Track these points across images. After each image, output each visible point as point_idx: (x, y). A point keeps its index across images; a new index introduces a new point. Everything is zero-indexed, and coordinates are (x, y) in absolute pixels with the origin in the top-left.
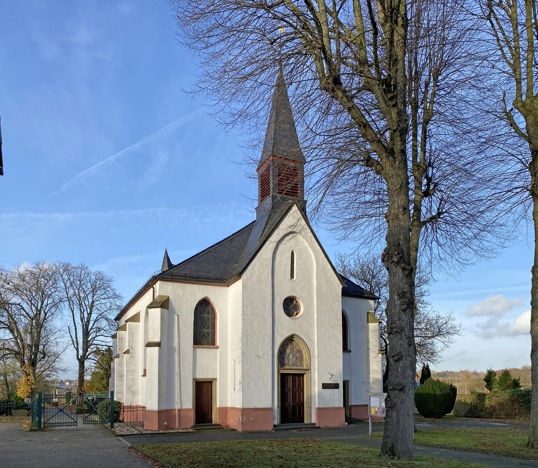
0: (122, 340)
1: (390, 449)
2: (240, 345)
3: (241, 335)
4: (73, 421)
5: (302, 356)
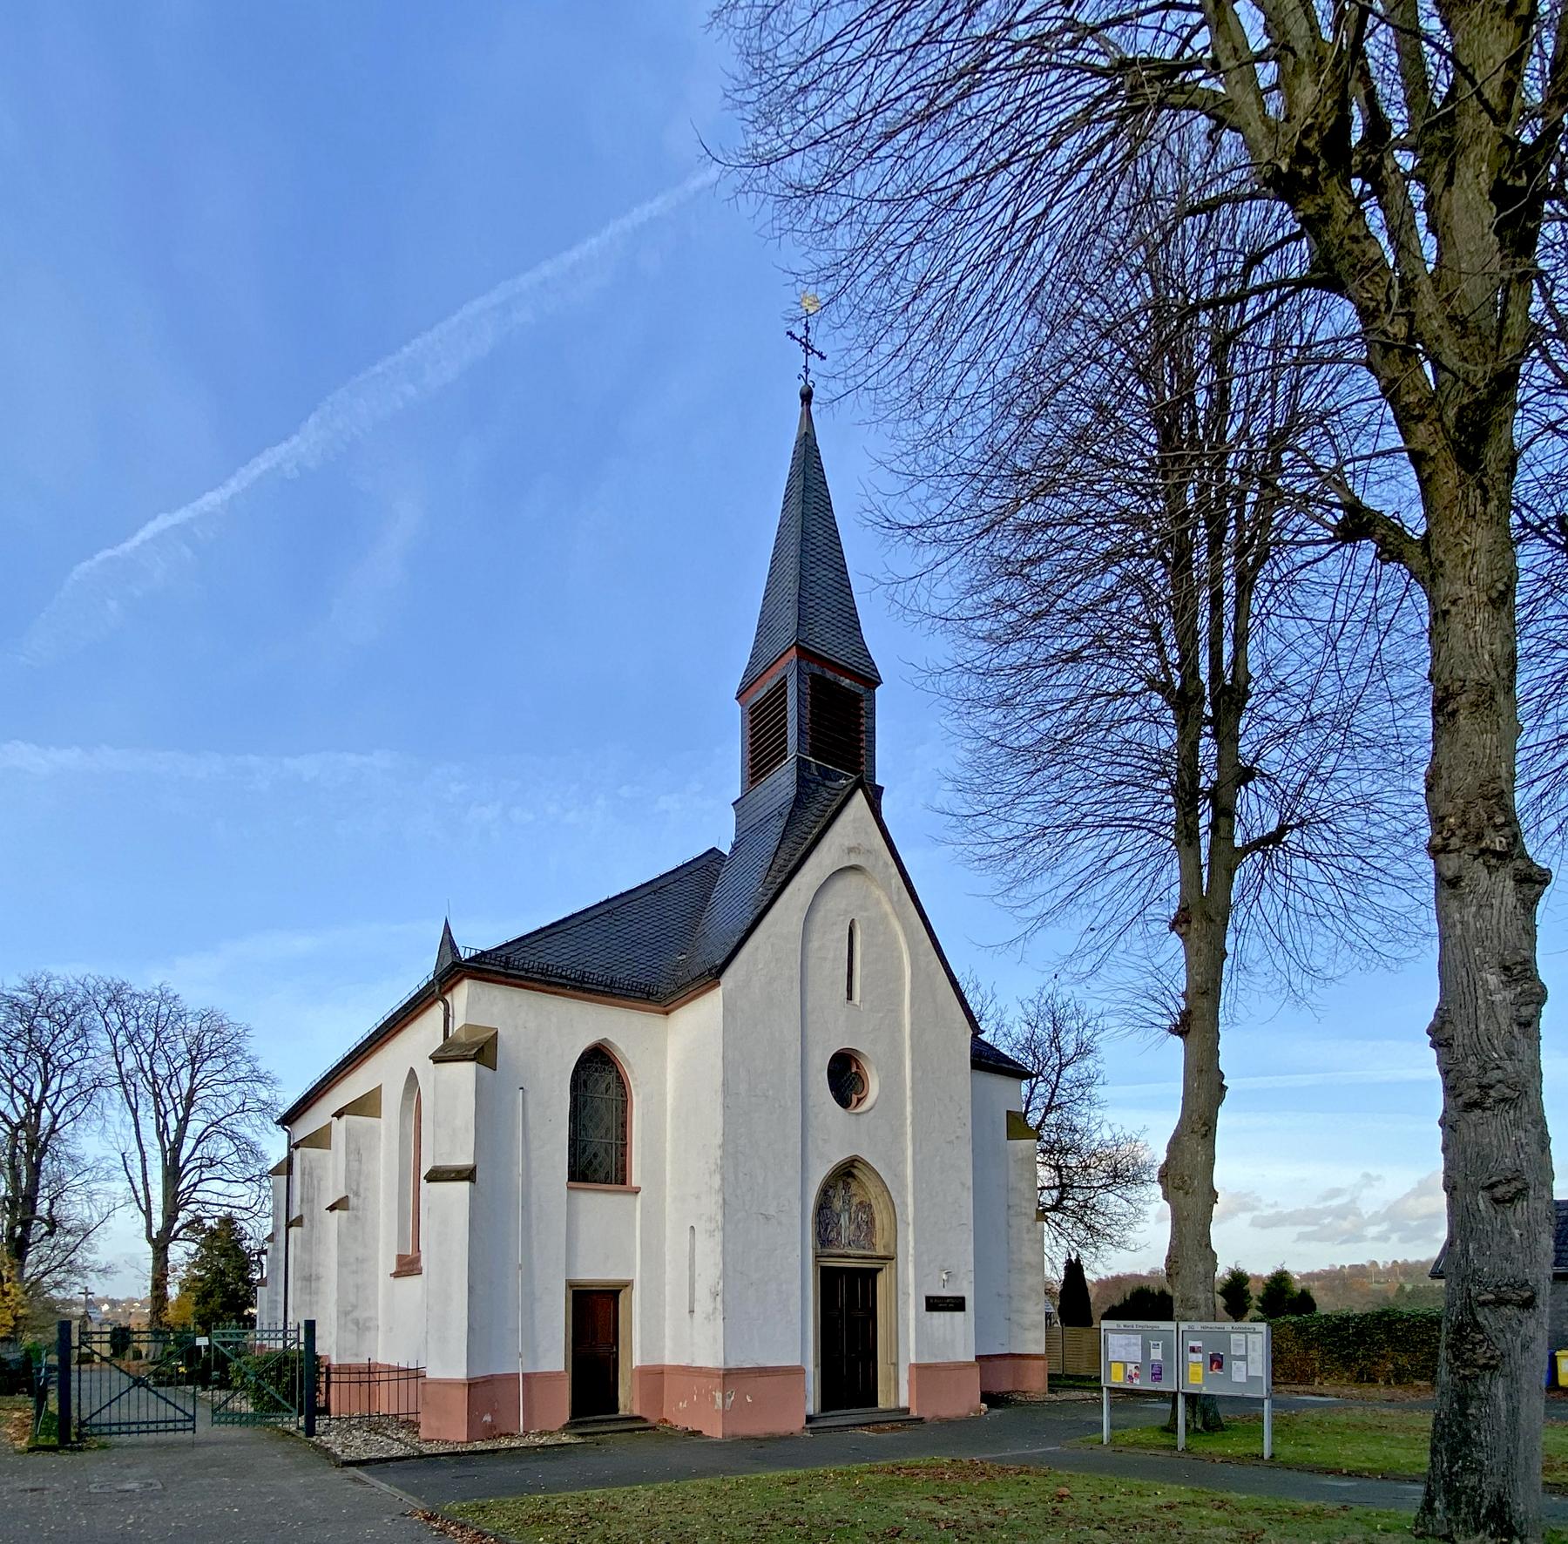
0: (311, 1174)
1: (1492, 1512)
2: (717, 1181)
3: (719, 1153)
4: (180, 1415)
5: (873, 1220)
